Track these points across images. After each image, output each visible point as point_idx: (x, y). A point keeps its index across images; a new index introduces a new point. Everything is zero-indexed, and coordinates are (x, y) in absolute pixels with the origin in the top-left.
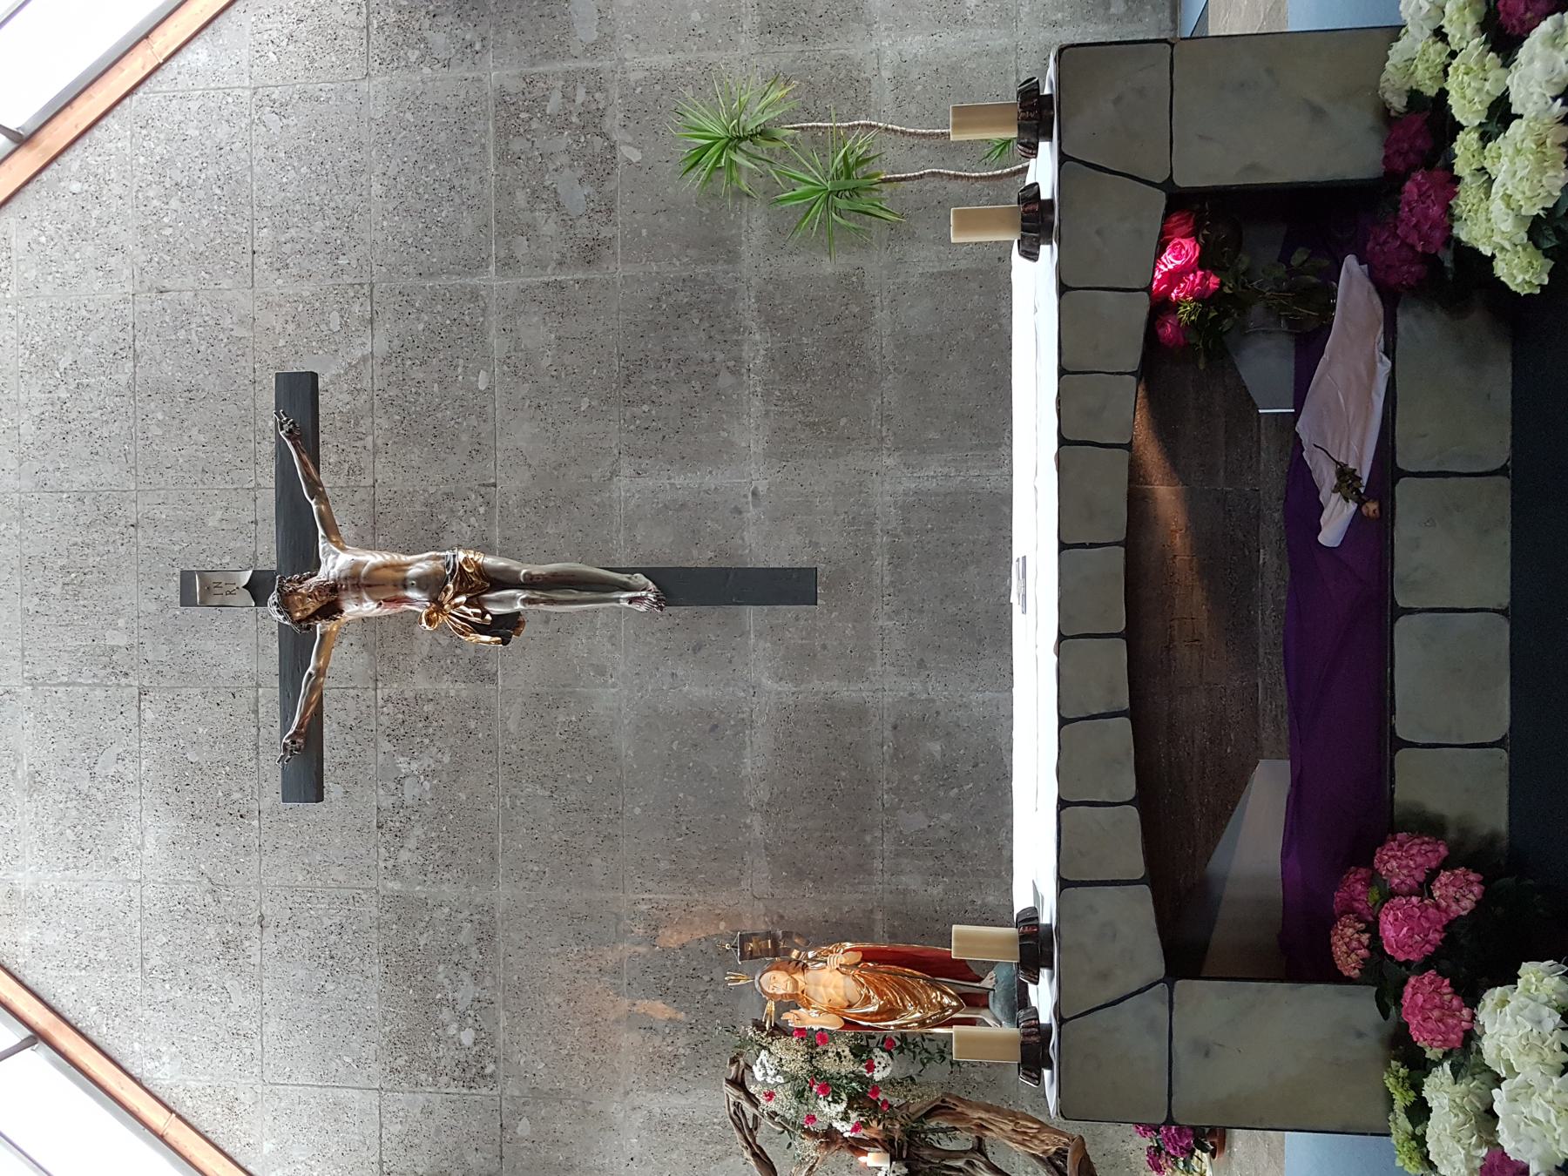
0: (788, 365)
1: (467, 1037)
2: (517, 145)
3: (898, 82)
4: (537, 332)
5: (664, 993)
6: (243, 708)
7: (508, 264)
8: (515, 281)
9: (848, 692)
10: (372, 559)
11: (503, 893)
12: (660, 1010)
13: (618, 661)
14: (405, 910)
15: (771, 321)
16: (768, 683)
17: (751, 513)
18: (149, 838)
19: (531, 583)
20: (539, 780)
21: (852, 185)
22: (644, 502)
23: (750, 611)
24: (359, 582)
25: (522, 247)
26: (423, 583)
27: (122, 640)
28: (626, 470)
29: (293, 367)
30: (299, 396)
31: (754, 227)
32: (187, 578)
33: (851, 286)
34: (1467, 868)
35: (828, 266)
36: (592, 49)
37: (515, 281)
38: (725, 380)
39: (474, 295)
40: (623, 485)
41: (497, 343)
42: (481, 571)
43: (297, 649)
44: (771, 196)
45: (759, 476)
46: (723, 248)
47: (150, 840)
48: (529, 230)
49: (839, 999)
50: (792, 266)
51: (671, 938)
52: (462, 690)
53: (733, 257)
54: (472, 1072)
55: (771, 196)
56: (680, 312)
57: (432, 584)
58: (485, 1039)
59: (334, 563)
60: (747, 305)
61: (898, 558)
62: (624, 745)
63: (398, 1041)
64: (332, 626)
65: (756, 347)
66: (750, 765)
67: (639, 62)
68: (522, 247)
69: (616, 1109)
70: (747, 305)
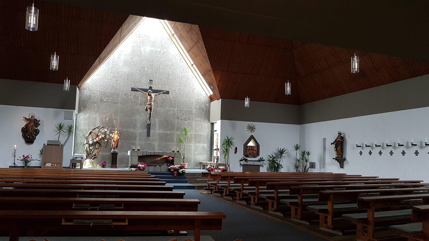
0: (167, 135)
1: (105, 100)
4: (171, 113)
5: (109, 120)
8: (176, 111)
9: (137, 139)
10: (153, 99)
11: (119, 105)
12: (107, 119)
13: (141, 118)
14: (118, 95)
15: (171, 134)
18: (126, 70)
19: (150, 113)
22: (156, 121)
23: (146, 131)
24: (151, 98)
25: (179, 112)
26: (151, 103)
30: (168, 93)
31: (179, 133)
32: (152, 81)
33: (173, 141)
34: (34, 32)
35: (175, 139)
36: (195, 119)
37: (176, 111)
40: (157, 119)
43: (146, 90)
48: (180, 113)
49: (85, 93)
50: (175, 136)
51: (114, 121)
53: (177, 131)
54: (101, 100)
55: (181, 135)
56: (172, 126)
57: (151, 104)
58: (105, 102)
59: (153, 95)
60: (172, 132)
62: (134, 118)
63: (105, 93)
65: (169, 132)
66: (131, 129)
67: (194, 124)
68: (179, 112)
69: (97, 114)
70: (172, 132)
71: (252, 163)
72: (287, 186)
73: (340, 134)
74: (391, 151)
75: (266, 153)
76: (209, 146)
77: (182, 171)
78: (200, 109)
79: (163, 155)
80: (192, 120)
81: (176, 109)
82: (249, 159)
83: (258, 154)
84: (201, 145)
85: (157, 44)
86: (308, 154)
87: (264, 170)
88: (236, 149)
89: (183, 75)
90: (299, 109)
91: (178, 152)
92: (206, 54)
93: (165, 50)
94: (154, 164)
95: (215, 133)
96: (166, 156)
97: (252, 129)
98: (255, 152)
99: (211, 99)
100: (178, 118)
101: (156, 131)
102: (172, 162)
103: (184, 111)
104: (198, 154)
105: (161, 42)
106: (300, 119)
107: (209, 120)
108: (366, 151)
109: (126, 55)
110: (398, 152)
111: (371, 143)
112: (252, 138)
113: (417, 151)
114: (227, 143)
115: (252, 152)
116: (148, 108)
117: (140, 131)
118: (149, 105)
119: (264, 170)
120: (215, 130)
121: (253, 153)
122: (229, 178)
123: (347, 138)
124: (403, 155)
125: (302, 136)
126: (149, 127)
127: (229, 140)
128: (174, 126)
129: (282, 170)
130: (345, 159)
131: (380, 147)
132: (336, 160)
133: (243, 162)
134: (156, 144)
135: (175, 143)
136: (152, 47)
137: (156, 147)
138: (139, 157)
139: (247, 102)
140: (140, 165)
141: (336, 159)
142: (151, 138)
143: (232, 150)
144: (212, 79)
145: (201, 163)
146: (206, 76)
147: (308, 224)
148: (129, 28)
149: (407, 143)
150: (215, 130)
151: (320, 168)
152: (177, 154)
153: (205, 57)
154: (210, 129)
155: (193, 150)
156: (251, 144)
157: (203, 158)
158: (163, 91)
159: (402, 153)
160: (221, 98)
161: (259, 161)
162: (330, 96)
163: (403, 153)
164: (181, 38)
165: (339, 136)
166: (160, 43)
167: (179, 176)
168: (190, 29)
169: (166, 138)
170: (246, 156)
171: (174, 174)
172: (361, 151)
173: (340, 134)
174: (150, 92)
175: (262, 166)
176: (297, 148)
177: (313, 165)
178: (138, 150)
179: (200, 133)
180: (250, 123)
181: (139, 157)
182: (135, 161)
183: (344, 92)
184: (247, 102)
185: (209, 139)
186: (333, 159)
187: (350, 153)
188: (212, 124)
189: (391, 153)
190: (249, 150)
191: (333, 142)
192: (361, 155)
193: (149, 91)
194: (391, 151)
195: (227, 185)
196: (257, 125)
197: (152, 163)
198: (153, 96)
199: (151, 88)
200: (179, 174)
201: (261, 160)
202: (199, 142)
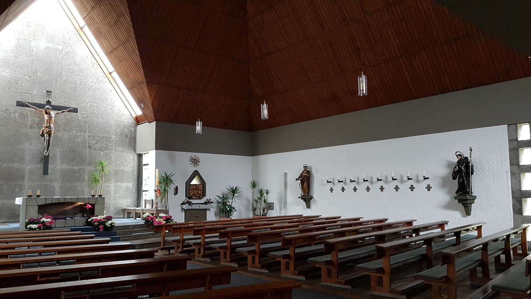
0: (74, 172)
2: (104, 139)
3: (108, 186)
4: (80, 139)
6: (27, 91)
7: (89, 136)
8: (87, 137)
9: (26, 178)
10: (53, 119)
13: (32, 147)
15: (80, 169)
16: (28, 167)
17: (54, 166)
19: (49, 140)
20: (14, 134)
21: (97, 181)
22: (56, 152)
24: (50, 118)
26: (50, 126)
27: (38, 75)
28: (60, 150)
29: (79, 110)
30: (75, 110)
31: (91, 168)
32: (51, 92)
33: (83, 180)
35: (86, 177)
36: (115, 149)
37: (87, 137)
38: (72, 164)
39: (85, 131)
40: (58, 149)
41: (79, 134)
42: (51, 134)
44: (96, 171)
45: (59, 167)
46: (89, 164)
47: (5, 74)
48: (93, 139)
50: (87, 173)
52: (29, 123)
53: (88, 165)
56: (81, 158)
57: (49, 127)
59: (53, 113)
60: (82, 167)
61: (46, 185)
62: (19, 147)
64: (44, 112)
65: (76, 168)
67: (113, 155)
70: (82, 167)
71: (197, 207)
72: (240, 233)
73: (306, 167)
74: (368, 187)
75: (213, 193)
76: (135, 185)
77: (111, 224)
78: (122, 134)
79: (76, 203)
80: (111, 150)
81: (87, 134)
82: (193, 201)
83: (204, 195)
84: (124, 185)
85: (57, 39)
86: (267, 193)
87: (211, 216)
88: (176, 189)
89: (96, 86)
90: (249, 135)
91: (100, 196)
92: (138, 60)
93: (69, 49)
94: (63, 215)
95: (144, 167)
96: (80, 203)
97: (195, 161)
98: (200, 193)
99: (138, 121)
100: (90, 147)
101: (57, 166)
102: (92, 212)
103: (99, 137)
104: (120, 197)
105: (63, 37)
106: (253, 150)
107: (135, 150)
108: (338, 187)
109: (7, 51)
110: (390, 187)
111: (344, 177)
112: (196, 174)
113: (397, 186)
114: (165, 181)
115: (196, 192)
116: (45, 132)
117: (30, 166)
118: (47, 127)
119: (211, 216)
120: (144, 164)
121: (198, 193)
122: (164, 227)
123: (313, 172)
124: (382, 191)
125: (256, 170)
126: (46, 161)
127: (167, 178)
128: (86, 157)
129: (235, 216)
130: (312, 198)
131: (354, 182)
132: (302, 199)
133: (185, 207)
134: (57, 185)
135: (86, 183)
136: (49, 42)
137: (57, 190)
138: (39, 206)
139: (199, 128)
140: (44, 219)
141: (303, 198)
142: (48, 177)
143: (171, 191)
144: (144, 94)
145: (124, 210)
146: (135, 89)
147: (350, 288)
148: (17, 10)
149: (402, 176)
150: (144, 163)
151: (281, 209)
152: (99, 199)
153: (136, 64)
154: (136, 163)
155: (113, 192)
156: (195, 182)
157: (127, 203)
158: (67, 108)
159: (395, 188)
160: (157, 120)
161: (206, 203)
162: (292, 122)
163: (397, 188)
164: (98, 34)
165: (305, 170)
166: (61, 37)
167: (106, 229)
168: (116, 23)
169: (72, 177)
170: (189, 198)
171: (99, 229)
172: (331, 188)
173: (306, 167)
174: (48, 108)
175: (209, 210)
176: (254, 185)
177: (270, 206)
178: (38, 196)
179: (122, 168)
180: (193, 154)
181: (39, 206)
182: (34, 214)
183: (309, 118)
184: (199, 128)
185: (136, 177)
186: (299, 197)
187: (318, 189)
188: (140, 156)
189: (368, 189)
190: (193, 189)
191: (297, 178)
192: (332, 192)
193: (46, 107)
194: (368, 187)
195: (225, 244)
196: (201, 156)
197: (58, 214)
198: (53, 115)
199: (49, 102)
200: (106, 228)
201: (209, 202)
202: (122, 181)
